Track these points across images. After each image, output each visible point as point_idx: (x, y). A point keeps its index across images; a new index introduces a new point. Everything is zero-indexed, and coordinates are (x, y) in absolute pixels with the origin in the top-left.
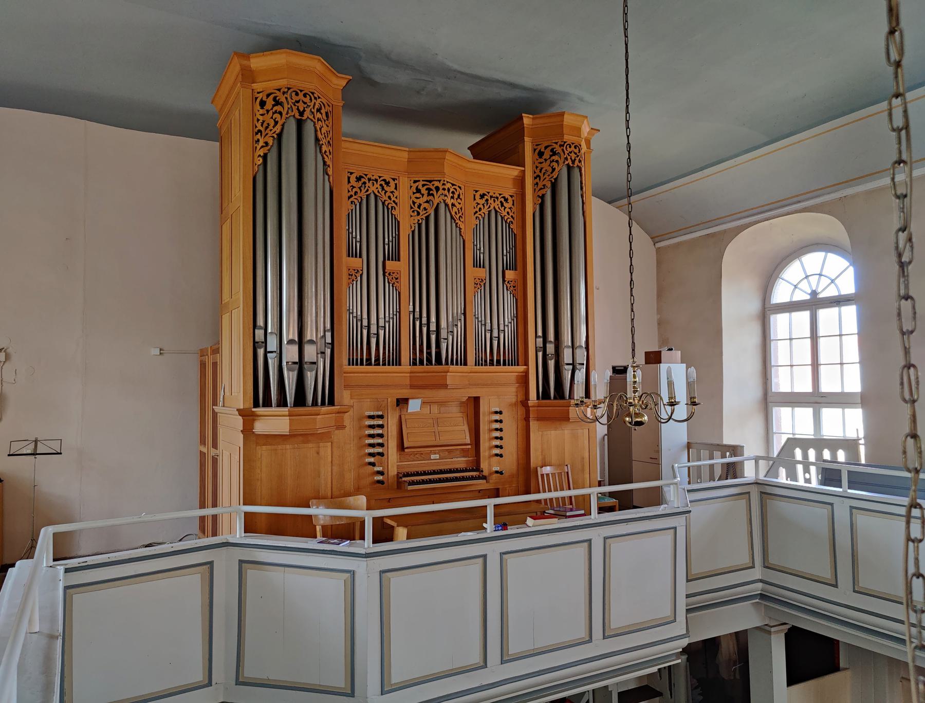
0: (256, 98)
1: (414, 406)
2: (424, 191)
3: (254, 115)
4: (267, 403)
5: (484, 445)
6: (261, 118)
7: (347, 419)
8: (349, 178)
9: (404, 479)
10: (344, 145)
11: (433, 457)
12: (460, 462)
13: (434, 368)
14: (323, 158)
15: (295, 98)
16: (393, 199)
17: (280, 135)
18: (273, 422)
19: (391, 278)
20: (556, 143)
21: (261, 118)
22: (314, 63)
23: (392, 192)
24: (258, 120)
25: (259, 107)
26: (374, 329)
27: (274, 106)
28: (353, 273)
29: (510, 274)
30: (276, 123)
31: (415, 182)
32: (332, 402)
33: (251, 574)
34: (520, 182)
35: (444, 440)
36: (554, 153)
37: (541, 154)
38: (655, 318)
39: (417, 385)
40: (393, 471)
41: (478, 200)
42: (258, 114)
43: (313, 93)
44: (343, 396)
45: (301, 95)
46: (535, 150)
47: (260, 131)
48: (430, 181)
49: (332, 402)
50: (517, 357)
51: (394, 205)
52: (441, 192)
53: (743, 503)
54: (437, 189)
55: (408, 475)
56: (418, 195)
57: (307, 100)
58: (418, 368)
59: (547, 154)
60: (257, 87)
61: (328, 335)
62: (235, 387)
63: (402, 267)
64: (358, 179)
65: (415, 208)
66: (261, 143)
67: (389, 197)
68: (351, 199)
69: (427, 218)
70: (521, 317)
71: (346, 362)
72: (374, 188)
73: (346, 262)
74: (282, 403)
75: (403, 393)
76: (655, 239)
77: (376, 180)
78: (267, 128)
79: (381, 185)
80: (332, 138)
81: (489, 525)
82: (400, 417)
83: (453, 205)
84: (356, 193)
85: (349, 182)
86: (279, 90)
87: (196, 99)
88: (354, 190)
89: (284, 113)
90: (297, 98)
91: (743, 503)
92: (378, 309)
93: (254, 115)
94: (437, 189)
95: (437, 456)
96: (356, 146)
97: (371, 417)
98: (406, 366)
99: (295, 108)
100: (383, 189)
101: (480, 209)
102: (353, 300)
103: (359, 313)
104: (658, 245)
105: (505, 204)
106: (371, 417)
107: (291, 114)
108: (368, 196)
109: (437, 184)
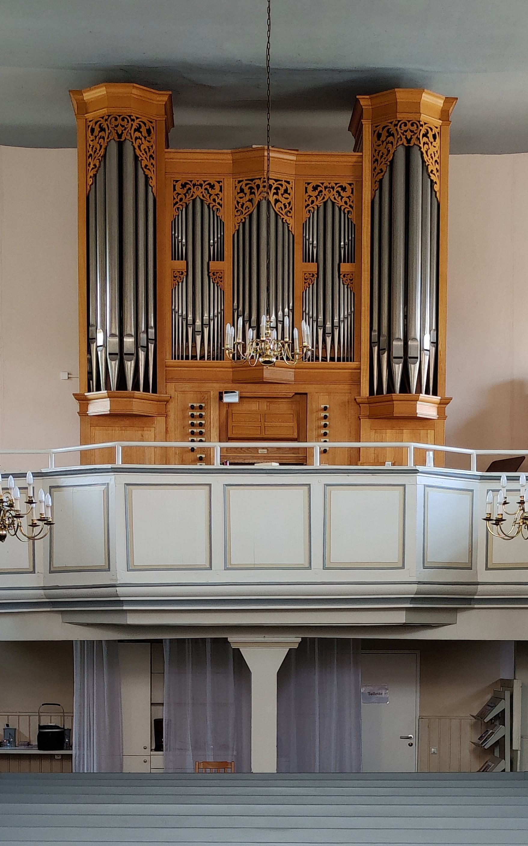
0: (89, 126)
2: (247, 190)
3: (87, 141)
4: (98, 389)
6: (91, 143)
8: (174, 186)
10: (167, 156)
14: (144, 172)
15: (114, 123)
16: (217, 201)
17: (104, 156)
19: (215, 277)
20: (391, 123)
21: (91, 143)
22: (135, 91)
23: (217, 195)
24: (90, 145)
25: (90, 134)
27: (99, 132)
28: (178, 274)
29: (346, 267)
30: (101, 146)
31: (239, 182)
34: (358, 167)
36: (390, 134)
37: (379, 136)
41: (310, 192)
42: (89, 140)
43: (130, 116)
44: (170, 389)
45: (120, 119)
46: (375, 132)
47: (91, 155)
48: (252, 180)
49: (155, 391)
50: (350, 355)
51: (219, 207)
52: (261, 189)
54: (258, 187)
56: (242, 195)
57: (414, 128)
59: (384, 134)
60: (89, 116)
61: (151, 331)
63: (225, 266)
64: (183, 186)
65: (239, 207)
66: (92, 166)
67: (214, 200)
68: (177, 206)
69: (251, 216)
71: (168, 356)
72: (198, 193)
73: (171, 266)
77: (201, 185)
78: (382, 156)
79: (338, 192)
80: (439, 157)
83: (277, 201)
84: (181, 200)
85: (175, 190)
86: (103, 118)
88: (180, 197)
89: (395, 143)
90: (117, 123)
93: (87, 141)
94: (258, 187)
96: (179, 156)
99: (403, 137)
100: (340, 195)
101: (313, 202)
103: (184, 313)
105: (342, 194)
107: (400, 143)
108: (325, 203)
109: (258, 182)
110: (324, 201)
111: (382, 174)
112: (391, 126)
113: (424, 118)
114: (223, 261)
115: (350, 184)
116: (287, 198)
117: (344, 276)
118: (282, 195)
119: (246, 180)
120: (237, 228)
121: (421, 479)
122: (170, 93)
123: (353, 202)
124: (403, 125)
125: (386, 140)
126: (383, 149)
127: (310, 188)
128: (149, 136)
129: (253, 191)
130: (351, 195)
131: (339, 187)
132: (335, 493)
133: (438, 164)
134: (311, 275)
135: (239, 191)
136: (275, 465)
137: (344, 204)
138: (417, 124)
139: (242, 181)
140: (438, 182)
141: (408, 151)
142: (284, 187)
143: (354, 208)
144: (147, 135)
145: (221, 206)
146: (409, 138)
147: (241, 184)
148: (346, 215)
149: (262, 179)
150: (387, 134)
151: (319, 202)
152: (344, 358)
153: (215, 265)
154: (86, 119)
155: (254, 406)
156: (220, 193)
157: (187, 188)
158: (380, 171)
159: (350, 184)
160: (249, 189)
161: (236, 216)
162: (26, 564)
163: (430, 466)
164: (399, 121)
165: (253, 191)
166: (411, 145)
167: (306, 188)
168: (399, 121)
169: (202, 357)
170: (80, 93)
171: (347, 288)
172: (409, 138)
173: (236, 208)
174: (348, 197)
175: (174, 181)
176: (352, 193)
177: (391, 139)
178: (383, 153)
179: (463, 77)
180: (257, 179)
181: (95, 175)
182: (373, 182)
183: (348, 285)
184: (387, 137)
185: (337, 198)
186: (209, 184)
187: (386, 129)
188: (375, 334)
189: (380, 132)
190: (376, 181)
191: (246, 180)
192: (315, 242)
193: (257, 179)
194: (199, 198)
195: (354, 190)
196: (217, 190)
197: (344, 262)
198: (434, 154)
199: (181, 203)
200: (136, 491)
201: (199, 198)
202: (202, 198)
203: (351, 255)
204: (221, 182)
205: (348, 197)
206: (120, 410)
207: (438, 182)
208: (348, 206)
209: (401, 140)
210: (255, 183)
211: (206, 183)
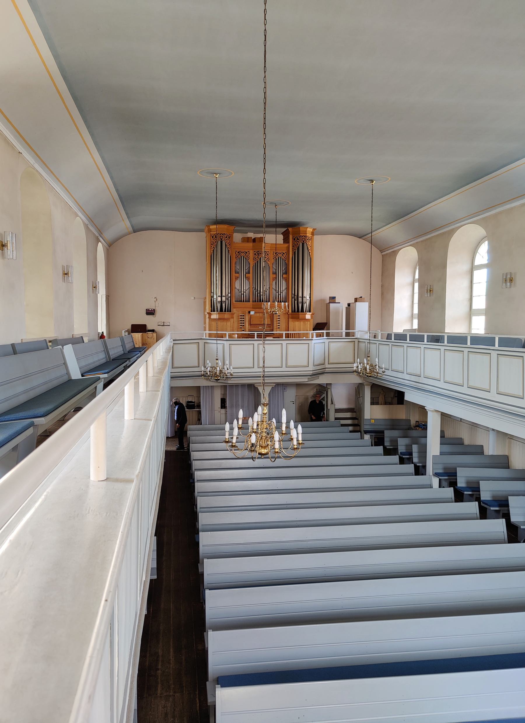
1: (252, 313)
4: (214, 311)
5: (275, 325)
7: (235, 316)
13: (259, 303)
18: (215, 316)
22: (225, 226)
26: (242, 293)
29: (285, 276)
32: (230, 311)
33: (206, 345)
34: (288, 248)
36: (298, 239)
37: (294, 239)
38: (381, 283)
39: (254, 308)
44: (234, 310)
49: (230, 311)
53: (352, 344)
58: (255, 303)
61: (229, 294)
62: (208, 308)
63: (251, 275)
64: (238, 253)
70: (287, 288)
71: (234, 301)
72: (242, 254)
73: (234, 274)
75: (249, 310)
76: (381, 251)
81: (256, 338)
87: (203, 227)
91: (352, 344)
92: (243, 286)
98: (251, 303)
102: (237, 285)
104: (383, 253)
113: (307, 235)
121: (313, 341)
132: (289, 346)
136: (272, 338)
138: (306, 237)
141: (303, 244)
155: (258, 315)
162: (197, 365)
163: (315, 338)
169: (243, 301)
182: (292, 252)
188: (293, 295)
200: (232, 346)
206: (221, 317)
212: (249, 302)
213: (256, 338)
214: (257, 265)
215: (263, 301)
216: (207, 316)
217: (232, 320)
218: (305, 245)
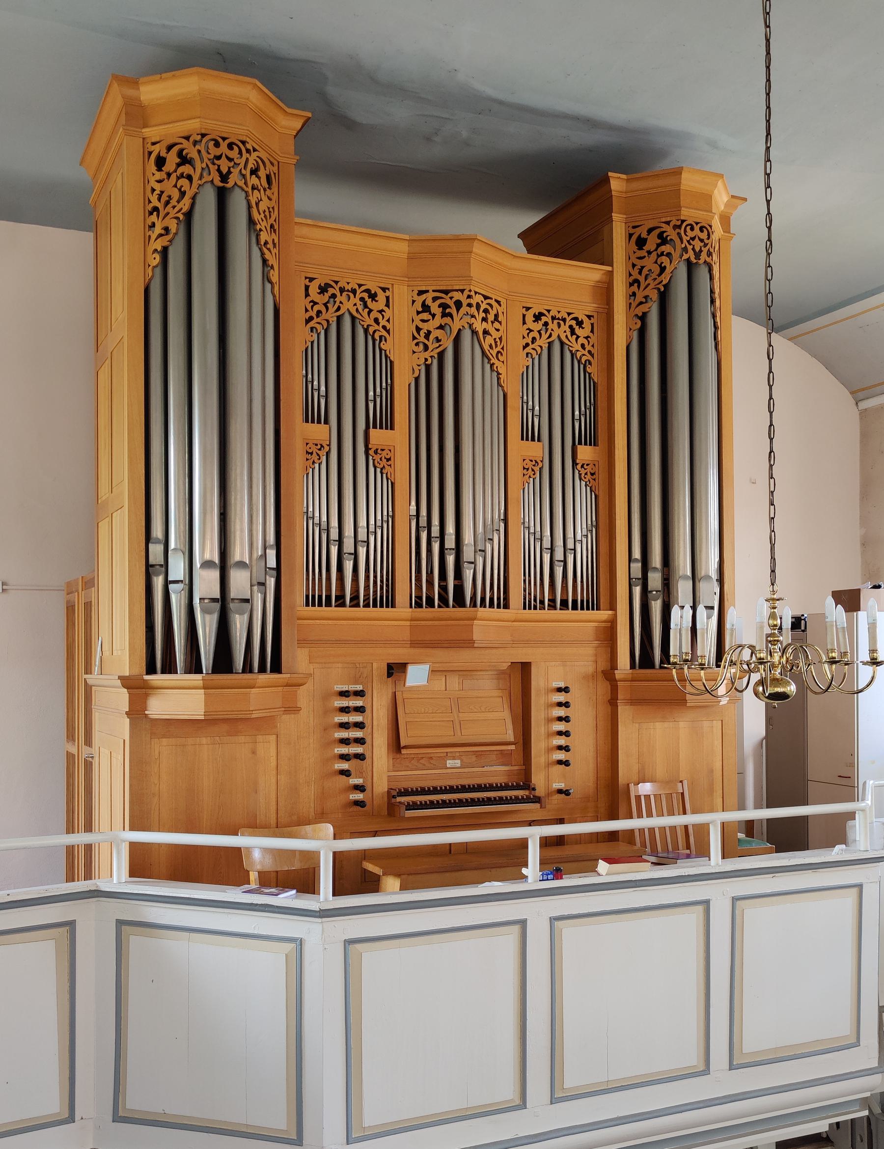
1: (417, 675)
2: (435, 308)
4: (169, 667)
6: (158, 187)
7: (304, 697)
8: (307, 288)
9: (399, 799)
10: (298, 231)
11: (450, 763)
12: (497, 772)
13: (452, 611)
14: (263, 254)
17: (189, 215)
18: (180, 697)
20: (668, 223)
21: (158, 187)
22: (246, 92)
23: (381, 311)
24: (153, 190)
29: (585, 453)
31: (421, 293)
32: (277, 668)
33: (136, 942)
34: (605, 291)
35: (470, 734)
37: (641, 243)
39: (423, 642)
40: (381, 786)
41: (530, 324)
44: (296, 657)
47: (156, 209)
48: (446, 292)
49: (277, 668)
51: (384, 333)
54: (459, 305)
55: (406, 793)
56: (425, 316)
57: (234, 154)
58: (425, 612)
61: (272, 554)
62: (118, 641)
63: (397, 440)
64: (323, 290)
65: (421, 338)
67: (376, 321)
68: (312, 324)
69: (441, 355)
70: (603, 527)
72: (349, 305)
73: (301, 433)
74: (194, 666)
76: (858, 394)
77: (354, 292)
79: (362, 299)
82: (394, 695)
83: (486, 332)
84: (319, 313)
85: (307, 295)
87: (55, 159)
88: (316, 308)
89: (195, 177)
92: (362, 513)
95: (458, 763)
97: (344, 694)
98: (403, 609)
99: (213, 168)
100: (366, 306)
101: (319, 313)
102: (313, 499)
103: (324, 518)
105: (578, 331)
106: (344, 694)
107: (207, 178)
109: (457, 296)
110: (338, 313)
111: (170, 236)
112: (665, 227)
114: (392, 428)
115: (589, 317)
116: (498, 330)
117: (376, 452)
118: (492, 323)
119: (434, 291)
120: (416, 375)
122: (310, 115)
123: (593, 346)
124: (689, 227)
125: (175, 171)
126: (649, 263)
127: (530, 318)
128: (270, 188)
129: (448, 310)
130: (591, 335)
131: (573, 319)
133: (275, 231)
134: (319, 447)
135: (420, 309)
137: (580, 349)
139: (427, 291)
140: (276, 268)
142: (495, 312)
143: (595, 356)
144: (267, 186)
145: (388, 332)
146: (224, 170)
147: (424, 296)
148: (377, 342)
149: (466, 293)
150: (659, 241)
151: (543, 342)
152: (575, 602)
153: (378, 436)
154: (144, 139)
156: (386, 309)
157: (330, 293)
158: (163, 232)
159: (589, 317)
160: (439, 306)
161: (414, 352)
164: (683, 221)
165: (448, 310)
166: (229, 185)
167: (524, 316)
168: (683, 221)
170: (134, 83)
171: (382, 473)
172: (224, 170)
173: (414, 338)
174: (587, 338)
175: (306, 278)
176: (592, 331)
177: (186, 169)
178: (170, 197)
179: (828, 179)
180: (457, 290)
181: (165, 252)
183: (382, 469)
184: (658, 245)
185: (360, 310)
186: (368, 291)
187: (175, 150)
188: (637, 567)
189: (163, 154)
190: (156, 250)
191: (434, 291)
192: (537, 408)
193: (457, 290)
194: (350, 314)
195: (595, 326)
196: (381, 304)
197: (375, 427)
198: (270, 212)
199: (319, 320)
201: (350, 314)
202: (355, 313)
203: (593, 432)
204: (388, 289)
205: (587, 338)
207: (276, 268)
208: (586, 353)
209: (687, 253)
210: (451, 298)
211: (363, 288)
212: (391, 603)
213: (715, 861)
214: (440, 384)
215: (474, 604)
216: (111, 701)
217: (287, 724)
218: (703, 272)
